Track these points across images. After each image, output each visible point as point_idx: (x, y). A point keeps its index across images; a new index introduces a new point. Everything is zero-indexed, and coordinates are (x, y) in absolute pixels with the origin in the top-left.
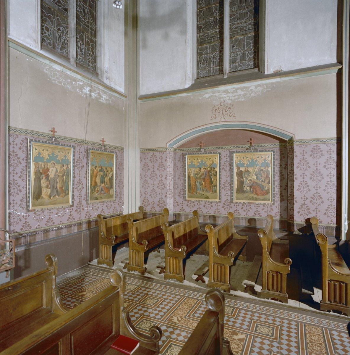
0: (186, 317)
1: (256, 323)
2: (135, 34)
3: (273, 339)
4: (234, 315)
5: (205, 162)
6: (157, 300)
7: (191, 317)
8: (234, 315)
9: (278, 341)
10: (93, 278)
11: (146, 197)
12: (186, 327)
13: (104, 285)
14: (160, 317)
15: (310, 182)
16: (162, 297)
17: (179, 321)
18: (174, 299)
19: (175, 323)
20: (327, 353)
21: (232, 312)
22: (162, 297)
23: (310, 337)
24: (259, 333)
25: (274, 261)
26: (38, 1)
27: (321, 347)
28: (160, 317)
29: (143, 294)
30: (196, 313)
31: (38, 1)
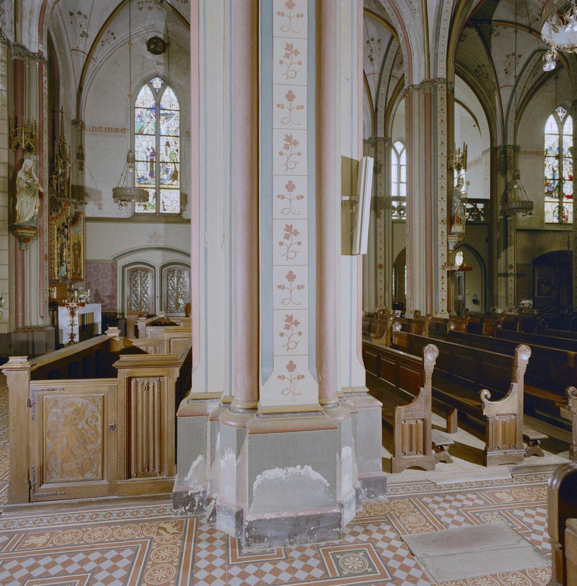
0: (149, 540)
1: (276, 553)
2: (140, 430)
3: (275, 556)
7: (140, 543)
9: (320, 549)
10: (532, 517)
12: (113, 541)
13: (537, 500)
16: (81, 571)
17: (160, 528)
18: (112, 563)
19: (168, 522)
24: (350, 574)
26: (352, 1)
30: (131, 558)
31: (352, 1)
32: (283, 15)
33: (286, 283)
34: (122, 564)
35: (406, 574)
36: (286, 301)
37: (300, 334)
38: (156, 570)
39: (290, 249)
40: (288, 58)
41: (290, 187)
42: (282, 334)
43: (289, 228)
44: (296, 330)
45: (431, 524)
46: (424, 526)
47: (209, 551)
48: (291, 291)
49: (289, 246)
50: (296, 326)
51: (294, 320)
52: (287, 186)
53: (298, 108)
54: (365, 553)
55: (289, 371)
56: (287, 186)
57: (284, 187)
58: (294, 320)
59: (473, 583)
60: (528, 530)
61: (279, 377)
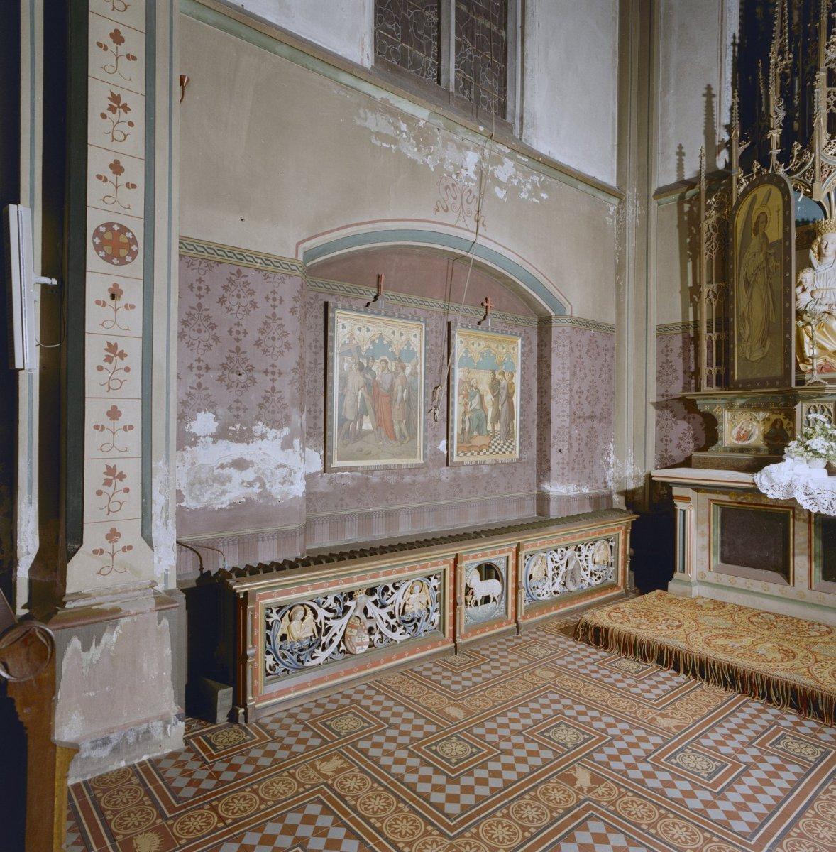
1: (752, 843)
4: (715, 785)
5: (390, 343)
6: (586, 737)
8: (715, 785)
11: (666, 450)
14: (590, 823)
15: (216, 312)
16: (604, 731)
20: (84, 840)
21: (711, 776)
22: (604, 731)
23: (651, 811)
25: (796, 242)
27: (245, 797)
28: (590, 823)
29: (549, 712)
32: (105, 180)
33: (107, 422)
34: (613, 751)
35: (330, 835)
36: (106, 570)
37: (127, 370)
38: (382, 811)
39: (116, 128)
40: (110, 363)
41: (114, 414)
42: (99, 493)
43: (112, 348)
44: (120, 485)
45: (413, 701)
46: (428, 693)
47: (747, 806)
48: (114, 433)
49: (111, 495)
50: (122, 359)
51: (117, 473)
52: (109, 414)
53: (125, 428)
54: (451, 763)
55: (114, 173)
56: (109, 414)
57: (105, 415)
58: (117, 473)
59: (203, 815)
60: (495, 752)
61: (95, 552)
